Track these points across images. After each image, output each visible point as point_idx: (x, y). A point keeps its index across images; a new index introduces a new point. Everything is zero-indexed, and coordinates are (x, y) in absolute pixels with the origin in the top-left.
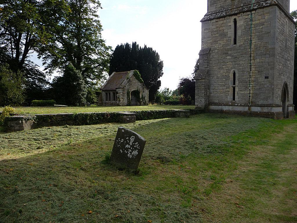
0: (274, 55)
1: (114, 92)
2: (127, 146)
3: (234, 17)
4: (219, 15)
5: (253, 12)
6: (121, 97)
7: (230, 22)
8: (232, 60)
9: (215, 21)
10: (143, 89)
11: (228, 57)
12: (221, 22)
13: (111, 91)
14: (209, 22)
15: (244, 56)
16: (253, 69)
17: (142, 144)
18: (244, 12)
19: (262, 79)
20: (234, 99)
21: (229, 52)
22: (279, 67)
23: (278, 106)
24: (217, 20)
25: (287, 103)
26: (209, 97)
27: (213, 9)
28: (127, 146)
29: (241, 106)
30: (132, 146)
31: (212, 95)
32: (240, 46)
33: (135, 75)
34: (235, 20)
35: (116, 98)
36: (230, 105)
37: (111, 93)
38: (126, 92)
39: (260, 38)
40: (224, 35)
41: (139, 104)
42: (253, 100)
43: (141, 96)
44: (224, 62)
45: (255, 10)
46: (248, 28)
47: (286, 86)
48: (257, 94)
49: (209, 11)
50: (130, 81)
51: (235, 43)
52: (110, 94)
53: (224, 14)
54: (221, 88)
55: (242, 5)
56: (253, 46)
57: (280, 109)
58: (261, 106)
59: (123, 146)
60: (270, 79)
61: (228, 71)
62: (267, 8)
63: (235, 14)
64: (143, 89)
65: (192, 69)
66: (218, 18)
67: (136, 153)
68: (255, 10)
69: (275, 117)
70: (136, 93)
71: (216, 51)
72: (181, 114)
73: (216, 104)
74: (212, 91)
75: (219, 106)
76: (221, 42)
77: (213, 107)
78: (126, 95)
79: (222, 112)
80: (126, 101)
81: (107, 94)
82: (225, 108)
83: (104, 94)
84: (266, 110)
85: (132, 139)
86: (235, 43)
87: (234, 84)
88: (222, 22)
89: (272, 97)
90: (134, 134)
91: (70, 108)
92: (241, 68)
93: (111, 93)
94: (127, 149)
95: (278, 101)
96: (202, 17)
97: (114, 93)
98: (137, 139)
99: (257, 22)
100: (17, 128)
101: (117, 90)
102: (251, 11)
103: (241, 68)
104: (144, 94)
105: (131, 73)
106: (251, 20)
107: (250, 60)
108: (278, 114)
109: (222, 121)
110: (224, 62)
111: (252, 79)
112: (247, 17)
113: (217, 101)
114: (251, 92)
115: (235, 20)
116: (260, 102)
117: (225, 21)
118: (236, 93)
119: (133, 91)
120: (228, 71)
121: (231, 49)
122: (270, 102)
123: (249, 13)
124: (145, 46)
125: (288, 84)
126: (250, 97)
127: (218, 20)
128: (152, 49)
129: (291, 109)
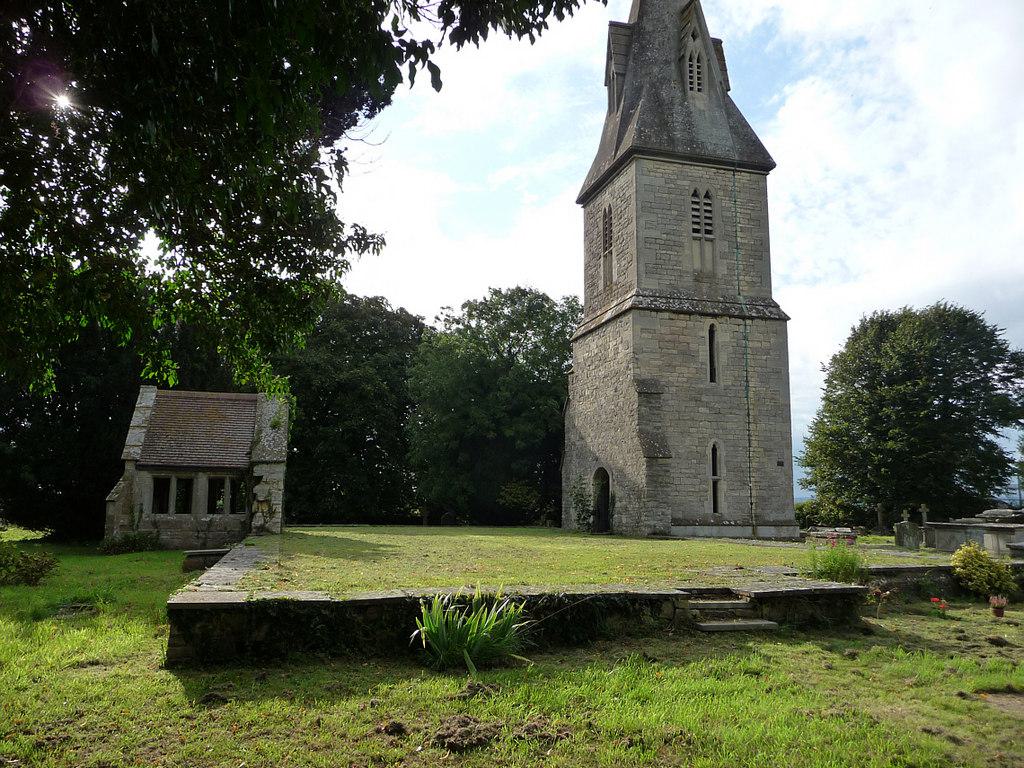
1: (219, 475)
3: (710, 321)
5: (748, 322)
8: (711, 418)
9: (666, 315)
11: (702, 410)
12: (682, 322)
16: (754, 444)
18: (731, 316)
19: (771, 467)
20: (715, 509)
21: (704, 398)
24: (673, 316)
27: (652, 284)
29: (736, 525)
32: (726, 388)
34: (712, 326)
36: (713, 525)
37: (202, 484)
40: (688, 355)
42: (759, 510)
46: (741, 353)
48: (764, 499)
53: (686, 306)
56: (751, 394)
62: (772, 322)
63: (714, 316)
66: (674, 312)
71: (674, 389)
86: (713, 379)
88: (684, 324)
92: (730, 437)
93: (202, 484)
101: (258, 471)
102: (744, 318)
106: (745, 338)
107: (749, 423)
115: (712, 326)
116: (772, 517)
120: (702, 441)
121: (706, 391)
123: (740, 321)
126: (752, 504)
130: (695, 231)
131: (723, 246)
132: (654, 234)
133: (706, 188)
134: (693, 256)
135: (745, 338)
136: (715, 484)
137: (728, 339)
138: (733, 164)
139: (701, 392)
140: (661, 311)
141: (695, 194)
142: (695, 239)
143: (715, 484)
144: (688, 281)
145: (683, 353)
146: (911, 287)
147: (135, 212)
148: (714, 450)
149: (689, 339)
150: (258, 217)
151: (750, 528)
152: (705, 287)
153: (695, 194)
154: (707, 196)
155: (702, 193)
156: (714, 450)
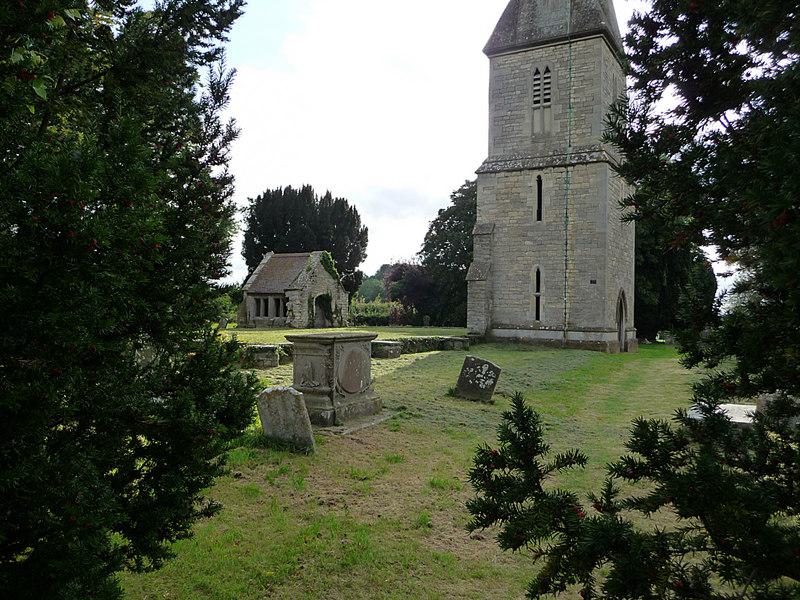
0: (604, 245)
1: (278, 297)
2: (479, 376)
4: (510, 166)
5: (570, 168)
6: (296, 309)
7: (530, 181)
8: (534, 249)
9: (502, 174)
10: (338, 291)
11: (527, 243)
12: (514, 178)
13: (271, 294)
14: (493, 175)
15: (556, 242)
16: (571, 266)
17: (497, 371)
19: (585, 285)
20: (538, 318)
22: (612, 263)
23: (611, 331)
24: (507, 174)
25: (625, 326)
26: (492, 312)
28: (479, 376)
29: (550, 329)
30: (486, 375)
31: (498, 309)
32: (549, 224)
33: (324, 262)
34: (539, 177)
35: (281, 312)
36: (531, 329)
37: (271, 300)
38: (306, 298)
39: (582, 214)
40: (519, 202)
41: (328, 323)
42: (571, 320)
43: (333, 307)
44: (519, 250)
45: (574, 165)
46: (562, 195)
47: (623, 294)
48: (577, 310)
49: (492, 155)
50: (308, 273)
51: (539, 218)
52: (266, 301)
53: (520, 164)
54: (512, 297)
55: (551, 153)
56: (569, 227)
57: (614, 337)
58: (584, 331)
59: (473, 376)
60: (598, 284)
61: (528, 267)
64: (338, 291)
65: (418, 243)
66: (508, 171)
67: (491, 382)
68: (574, 165)
69: (608, 349)
70: (324, 301)
72: (456, 344)
73: (504, 327)
74: (497, 302)
75: (513, 331)
76: (515, 214)
77: (498, 332)
78: (306, 304)
79: (516, 340)
80: (305, 318)
81: (258, 301)
82: (523, 334)
83: (250, 301)
84: (592, 337)
85: (485, 368)
86: (539, 218)
87: (538, 290)
89: (602, 316)
90: (487, 363)
91: (433, 330)
92: (550, 262)
93: (271, 300)
94: (479, 379)
95: (612, 322)
96: (478, 165)
97: (277, 301)
98: (491, 367)
99: (576, 186)
100: (268, 363)
101: (287, 294)
102: (566, 166)
103: (550, 262)
104: (339, 302)
105: (315, 257)
106: (567, 182)
108: (612, 344)
109: (530, 355)
110: (519, 250)
111: (570, 283)
112: (560, 175)
113: (507, 322)
114: (568, 305)
115: (539, 177)
117: (521, 178)
118: (541, 307)
119: (320, 296)
120: (528, 267)
121: (532, 229)
122: (598, 323)
124: (328, 195)
125: (626, 291)
127: (510, 174)
128: (307, 191)
129: (631, 335)
130: (548, 100)
131: (558, 109)
132: (502, 113)
133: (545, 64)
134: (547, 121)
135: (567, 182)
136: (538, 299)
137: (551, 185)
138: (566, 39)
139: (527, 229)
140: (499, 172)
141: (537, 72)
142: (535, 109)
143: (538, 299)
144: (528, 143)
145: (514, 202)
146: (277, 182)
147: (681, 18)
148: (538, 273)
149: (519, 190)
150: (675, 40)
151: (562, 333)
152: (540, 146)
153: (537, 72)
154: (547, 70)
155: (542, 70)
156: (538, 273)
